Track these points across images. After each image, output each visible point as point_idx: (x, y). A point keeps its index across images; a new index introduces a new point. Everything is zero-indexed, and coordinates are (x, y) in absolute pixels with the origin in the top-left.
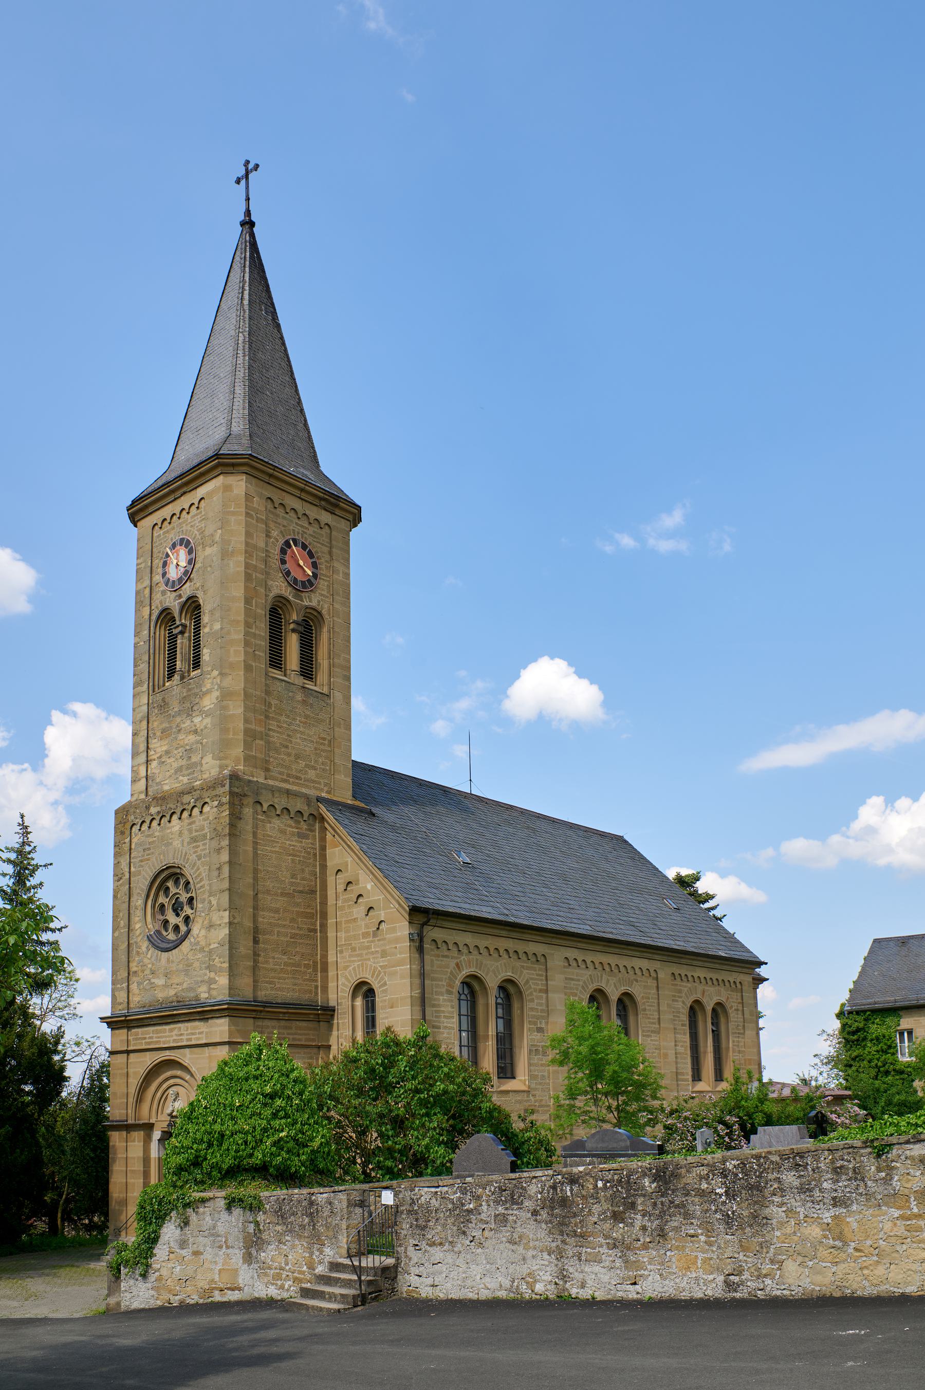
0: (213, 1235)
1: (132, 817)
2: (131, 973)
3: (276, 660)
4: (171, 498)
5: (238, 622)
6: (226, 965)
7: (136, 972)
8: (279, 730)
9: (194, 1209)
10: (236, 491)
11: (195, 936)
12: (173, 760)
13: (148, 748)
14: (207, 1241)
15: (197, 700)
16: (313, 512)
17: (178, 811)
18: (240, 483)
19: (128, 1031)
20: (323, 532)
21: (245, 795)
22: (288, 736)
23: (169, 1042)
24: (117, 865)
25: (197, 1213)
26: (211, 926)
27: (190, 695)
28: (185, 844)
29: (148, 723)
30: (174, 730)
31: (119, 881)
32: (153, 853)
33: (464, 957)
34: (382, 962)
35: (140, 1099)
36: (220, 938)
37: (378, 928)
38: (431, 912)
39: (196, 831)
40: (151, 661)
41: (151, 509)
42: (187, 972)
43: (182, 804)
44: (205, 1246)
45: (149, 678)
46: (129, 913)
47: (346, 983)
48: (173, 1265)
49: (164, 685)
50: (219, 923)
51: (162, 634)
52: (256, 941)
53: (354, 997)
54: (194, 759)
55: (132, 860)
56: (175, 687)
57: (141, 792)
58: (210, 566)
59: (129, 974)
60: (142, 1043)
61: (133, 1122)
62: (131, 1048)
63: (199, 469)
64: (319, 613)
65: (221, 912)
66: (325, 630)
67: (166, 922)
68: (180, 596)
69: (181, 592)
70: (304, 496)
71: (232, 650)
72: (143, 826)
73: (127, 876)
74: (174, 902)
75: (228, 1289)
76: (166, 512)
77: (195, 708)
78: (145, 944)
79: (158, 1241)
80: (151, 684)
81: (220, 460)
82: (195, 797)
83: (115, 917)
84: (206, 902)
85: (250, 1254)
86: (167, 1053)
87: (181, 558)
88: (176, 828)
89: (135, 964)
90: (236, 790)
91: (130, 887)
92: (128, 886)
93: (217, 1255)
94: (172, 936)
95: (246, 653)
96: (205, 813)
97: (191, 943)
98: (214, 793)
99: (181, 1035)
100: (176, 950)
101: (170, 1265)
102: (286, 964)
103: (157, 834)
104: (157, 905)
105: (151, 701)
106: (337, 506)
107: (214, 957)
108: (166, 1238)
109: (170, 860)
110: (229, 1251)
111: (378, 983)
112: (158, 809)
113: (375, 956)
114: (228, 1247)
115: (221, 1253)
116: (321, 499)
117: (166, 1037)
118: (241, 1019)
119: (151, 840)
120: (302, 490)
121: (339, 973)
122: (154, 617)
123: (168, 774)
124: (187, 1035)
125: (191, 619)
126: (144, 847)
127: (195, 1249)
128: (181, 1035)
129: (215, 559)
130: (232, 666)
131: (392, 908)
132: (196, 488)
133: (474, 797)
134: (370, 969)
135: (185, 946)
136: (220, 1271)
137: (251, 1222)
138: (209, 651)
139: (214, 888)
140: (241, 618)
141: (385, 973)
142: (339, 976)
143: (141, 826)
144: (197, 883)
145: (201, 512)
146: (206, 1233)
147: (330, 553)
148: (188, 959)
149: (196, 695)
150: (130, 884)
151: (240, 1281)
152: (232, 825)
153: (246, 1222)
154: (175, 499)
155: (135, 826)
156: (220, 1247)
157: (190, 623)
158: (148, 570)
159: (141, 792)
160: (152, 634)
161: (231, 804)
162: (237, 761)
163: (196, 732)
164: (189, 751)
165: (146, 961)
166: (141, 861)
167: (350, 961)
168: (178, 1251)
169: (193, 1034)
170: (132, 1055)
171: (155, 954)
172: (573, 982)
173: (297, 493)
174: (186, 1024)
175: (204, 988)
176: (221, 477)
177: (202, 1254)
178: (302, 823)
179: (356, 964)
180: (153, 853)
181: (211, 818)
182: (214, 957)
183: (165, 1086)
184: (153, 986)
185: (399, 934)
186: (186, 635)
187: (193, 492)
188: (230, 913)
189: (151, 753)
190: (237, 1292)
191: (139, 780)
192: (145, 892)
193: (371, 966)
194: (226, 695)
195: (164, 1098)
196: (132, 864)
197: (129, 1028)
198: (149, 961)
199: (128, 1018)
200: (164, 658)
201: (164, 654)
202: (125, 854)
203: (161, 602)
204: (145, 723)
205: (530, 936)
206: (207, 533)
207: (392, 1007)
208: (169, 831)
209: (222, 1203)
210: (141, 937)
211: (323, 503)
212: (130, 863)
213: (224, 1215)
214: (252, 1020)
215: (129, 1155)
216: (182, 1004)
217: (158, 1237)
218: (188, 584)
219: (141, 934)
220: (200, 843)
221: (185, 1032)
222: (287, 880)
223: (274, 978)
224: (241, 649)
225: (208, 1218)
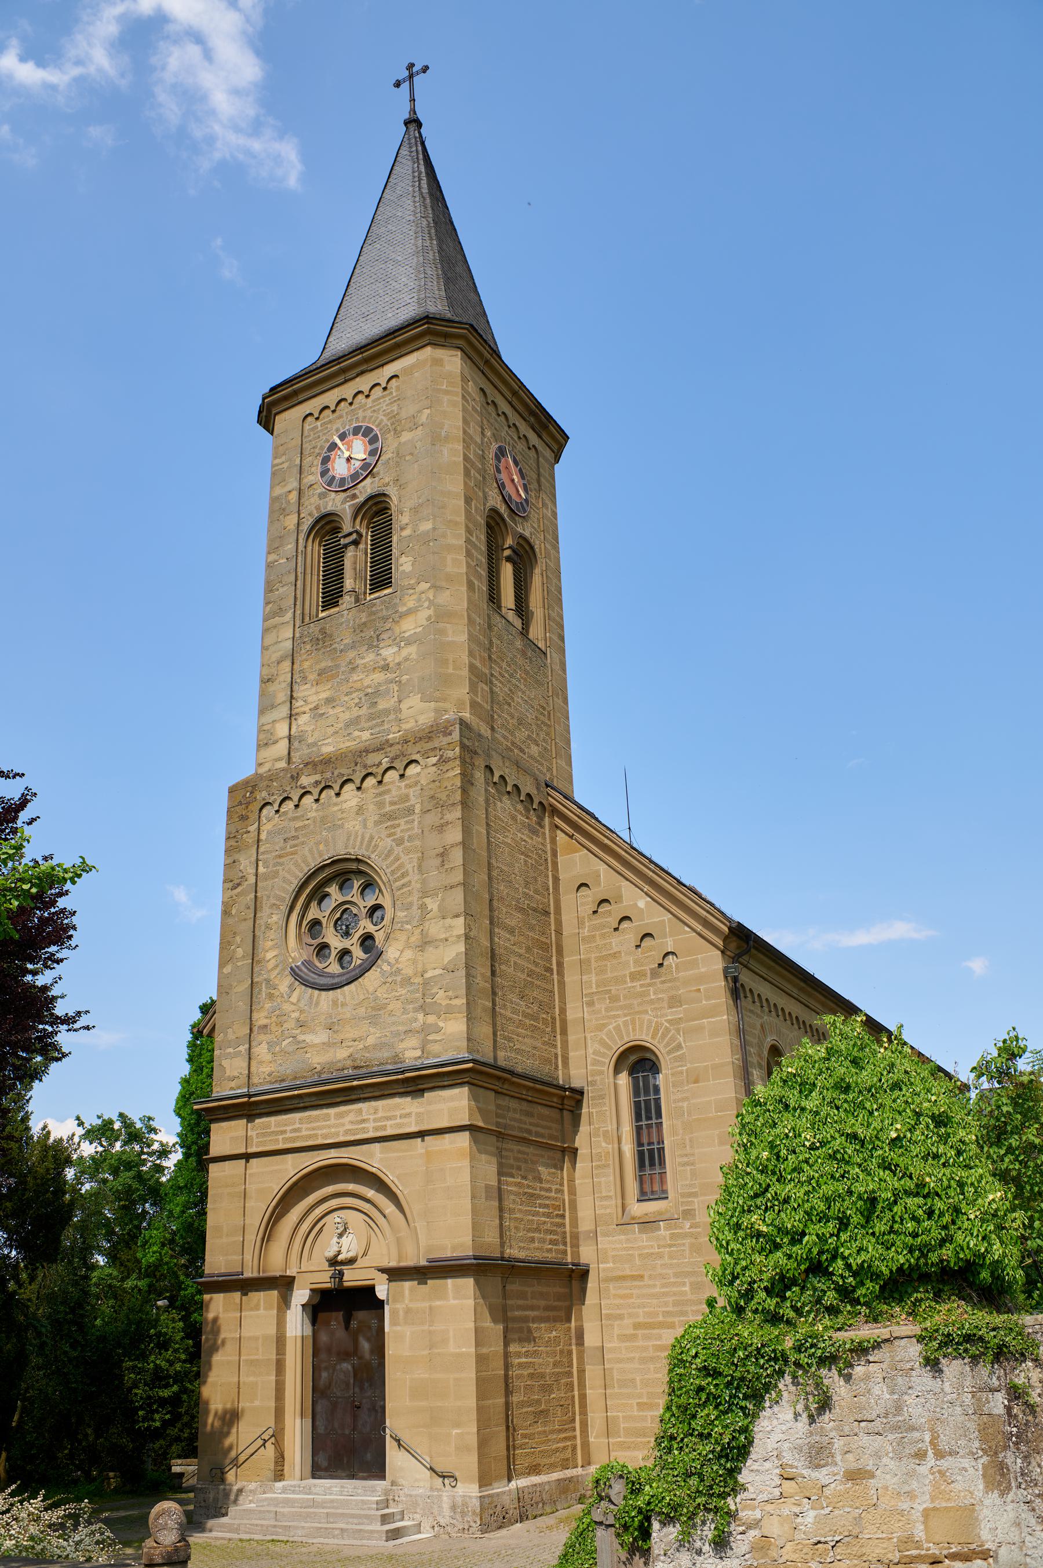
0: (896, 1428)
1: (264, 794)
2: (255, 1029)
4: (341, 379)
5: (456, 523)
6: (462, 1001)
7: (266, 1026)
9: (840, 1371)
10: (448, 368)
11: (393, 961)
12: (342, 709)
13: (292, 697)
14: (885, 1443)
15: (388, 626)
17: (357, 778)
18: (454, 359)
19: (248, 1122)
22: (511, 690)
23: (337, 1134)
24: (230, 866)
25: (848, 1378)
26: (425, 943)
27: (374, 620)
28: (370, 824)
29: (293, 663)
30: (343, 669)
31: (234, 888)
32: (303, 843)
34: (672, 1014)
35: (268, 1234)
36: (446, 960)
37: (661, 965)
39: (392, 803)
40: (299, 583)
41: (301, 397)
42: (373, 1020)
43: (365, 766)
44: (877, 1455)
45: (295, 605)
46: (254, 936)
47: (603, 1050)
48: (797, 1510)
49: (317, 616)
50: (443, 936)
51: (315, 551)
53: (617, 1071)
54: (382, 705)
55: (260, 857)
56: (346, 612)
57: (280, 759)
58: (411, 454)
59: (251, 1030)
60: (277, 1140)
61: (255, 1275)
62: (250, 1151)
63: (395, 337)
64: (532, 548)
65: (448, 921)
66: (537, 571)
67: (323, 949)
68: (354, 496)
69: (356, 491)
70: (515, 402)
71: (449, 558)
72: (283, 806)
73: (252, 880)
74: (338, 915)
75: (953, 1557)
76: (330, 398)
77: (384, 636)
78: (285, 983)
79: (748, 1453)
80: (298, 612)
81: (432, 326)
82: (391, 755)
83: (225, 944)
84: (415, 907)
85: (1002, 1468)
86: (333, 1153)
87: (359, 449)
88: (354, 802)
89: (263, 1014)
91: (256, 897)
92: (252, 896)
93: (911, 1474)
94: (335, 968)
95: (468, 565)
96: (410, 777)
97: (383, 972)
98: (430, 745)
99: (363, 1121)
100: (352, 985)
101: (788, 1508)
103: (313, 814)
104: (305, 923)
105: (297, 635)
106: (545, 428)
107: (434, 991)
108: (771, 1444)
109: (340, 849)
110: (945, 1463)
111: (665, 1047)
112: (312, 779)
113: (656, 1005)
114: (939, 1455)
115: (923, 1470)
117: (329, 1127)
119: (299, 824)
121: (588, 1036)
122: (305, 527)
123: (330, 730)
124: (375, 1120)
125: (368, 528)
126: (286, 836)
127: (854, 1466)
128: (363, 1121)
129: (418, 444)
130: (450, 579)
131: (687, 932)
132: (382, 365)
134: (649, 1027)
135: (372, 978)
136: (926, 1513)
137: (994, 1390)
138: (411, 558)
139: (432, 884)
140: (461, 518)
141: (678, 1031)
142: (589, 1042)
143: (280, 806)
144: (396, 880)
145: (391, 393)
146: (877, 1425)
147: (539, 482)
148: (376, 999)
149: (385, 619)
150: (256, 892)
151: (985, 1535)
152: (464, 791)
153: (981, 1390)
154: (346, 381)
155: (268, 807)
156: (921, 1455)
157: (367, 533)
158: (296, 470)
159: (280, 759)
160: (301, 548)
161: (463, 762)
162: (460, 704)
163: (386, 668)
164: (372, 696)
165: (287, 1007)
166: (280, 856)
167: (609, 1017)
168: (805, 1472)
169: (388, 1118)
170: (253, 1162)
171: (307, 996)
174: (373, 1103)
175: (413, 1042)
176: (429, 349)
177: (873, 1476)
178: (532, 812)
179: (620, 1021)
180: (303, 843)
181: (424, 782)
182: (434, 991)
183: (318, 1211)
184: (302, 1047)
185: (703, 970)
186: (362, 546)
187: (376, 371)
188: (465, 919)
189: (297, 704)
190: (979, 1562)
191: (276, 742)
192: (288, 901)
193: (650, 1022)
194: (442, 615)
195: (317, 1229)
196: (260, 863)
197: (251, 1117)
198: (293, 1007)
199: (253, 1099)
200: (319, 581)
201: (318, 575)
202: (248, 847)
203: (318, 508)
204: (287, 664)
206: (404, 415)
207: (696, 1081)
208: (336, 808)
209: (914, 1351)
210: (276, 972)
211: (532, 419)
212: (257, 860)
213: (923, 1379)
214: (493, 1093)
215: (245, 1333)
216: (364, 1070)
217: (750, 1443)
218: (369, 480)
219: (277, 966)
220: (402, 821)
221: (371, 1117)
224: (462, 557)
225: (880, 1390)
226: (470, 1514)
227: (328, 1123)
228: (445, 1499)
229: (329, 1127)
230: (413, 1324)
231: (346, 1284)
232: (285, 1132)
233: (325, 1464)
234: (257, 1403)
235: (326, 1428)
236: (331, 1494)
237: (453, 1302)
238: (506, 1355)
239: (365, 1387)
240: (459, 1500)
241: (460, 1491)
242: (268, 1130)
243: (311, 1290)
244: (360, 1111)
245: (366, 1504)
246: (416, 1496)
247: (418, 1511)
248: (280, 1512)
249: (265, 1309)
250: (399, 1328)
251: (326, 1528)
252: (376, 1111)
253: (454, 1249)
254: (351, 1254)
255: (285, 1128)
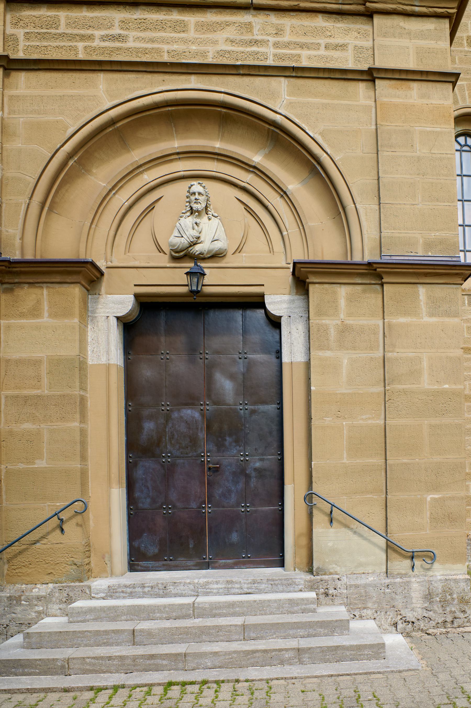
60: (75, 49)
117: (185, 41)
221: (272, 39)
226: (456, 602)
227: (182, 35)
228: (415, 586)
229: (185, 41)
230: (354, 348)
231: (208, 290)
232: (90, 38)
233: (153, 550)
234: (41, 464)
235: (154, 501)
236: (207, 594)
237: (427, 319)
238: (84, 457)
239: (227, 443)
240: (438, 587)
241: (437, 574)
242: (53, 31)
243: (137, 296)
244: (249, 27)
245: (298, 605)
246: (365, 586)
247: (370, 605)
248: (141, 631)
249: (53, 315)
250: (328, 354)
251: (265, 651)
252: (279, 32)
253: (428, 245)
254: (218, 246)
255: (89, 32)
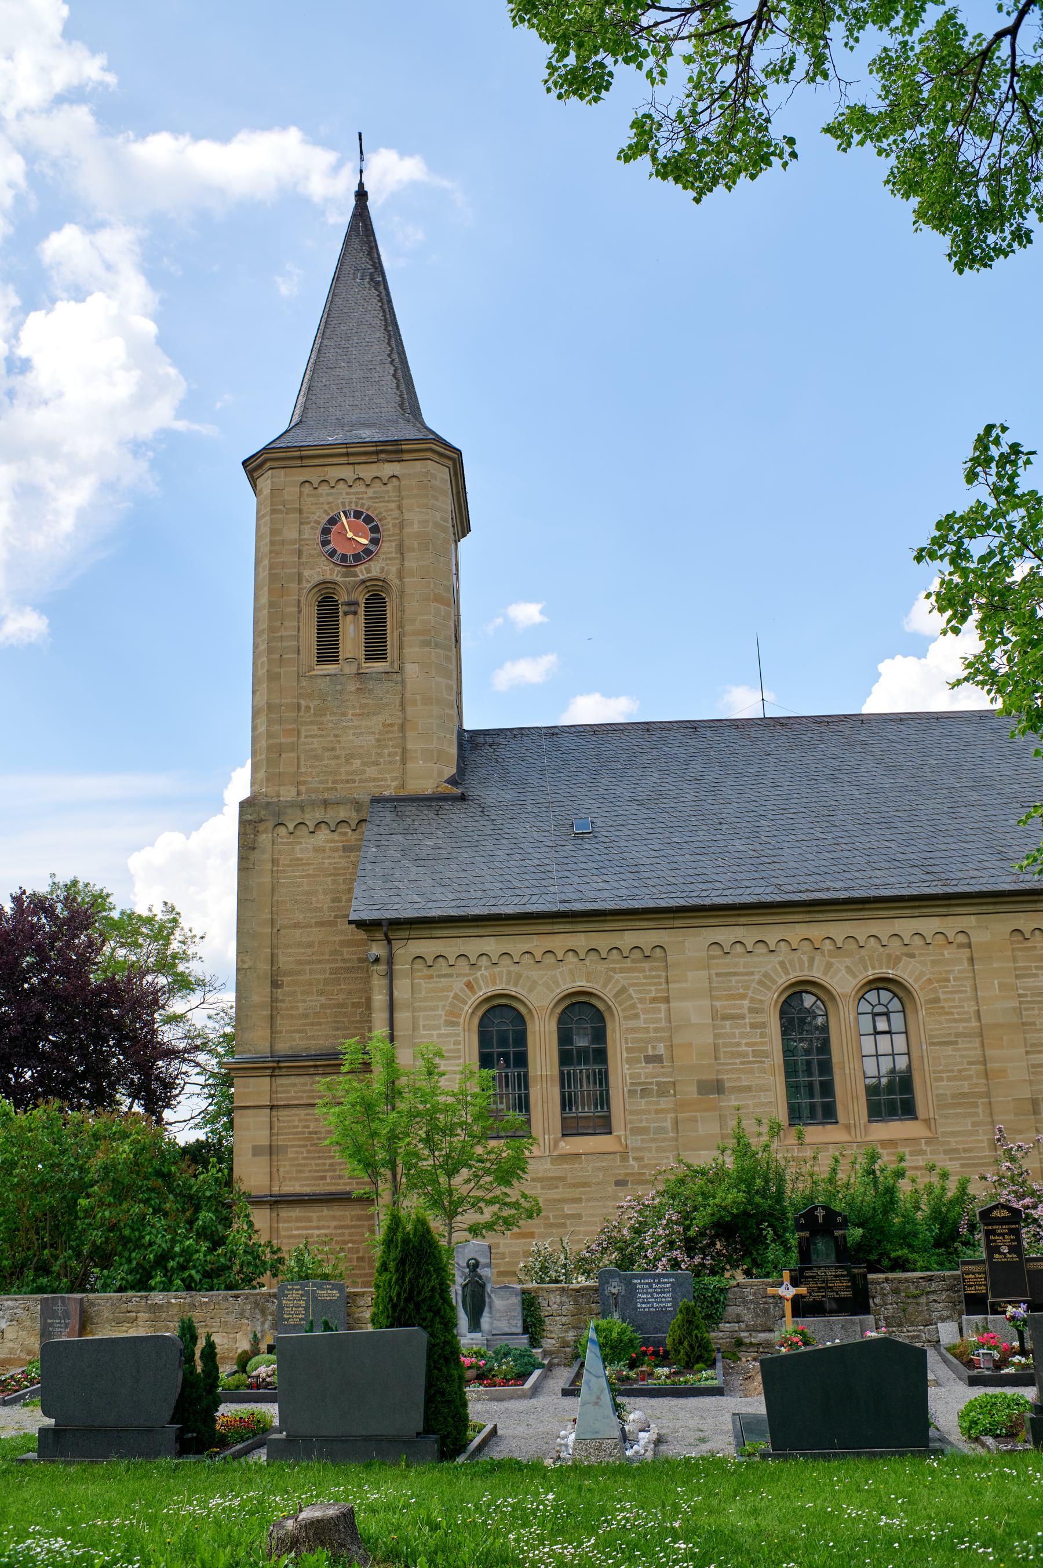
3: (328, 651)
8: (321, 733)
16: (367, 472)
20: (389, 487)
21: (261, 821)
33: (483, 971)
38: (384, 923)
52: (275, 984)
70: (352, 460)
90: (249, 817)
102: (322, 1006)
116: (377, 453)
118: (251, 1079)
120: (347, 455)
133: (771, 722)
172: (734, 979)
173: (344, 460)
205: (620, 924)
211: (383, 456)
222: (326, 907)
223: (305, 1025)
